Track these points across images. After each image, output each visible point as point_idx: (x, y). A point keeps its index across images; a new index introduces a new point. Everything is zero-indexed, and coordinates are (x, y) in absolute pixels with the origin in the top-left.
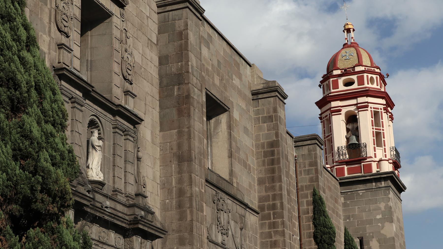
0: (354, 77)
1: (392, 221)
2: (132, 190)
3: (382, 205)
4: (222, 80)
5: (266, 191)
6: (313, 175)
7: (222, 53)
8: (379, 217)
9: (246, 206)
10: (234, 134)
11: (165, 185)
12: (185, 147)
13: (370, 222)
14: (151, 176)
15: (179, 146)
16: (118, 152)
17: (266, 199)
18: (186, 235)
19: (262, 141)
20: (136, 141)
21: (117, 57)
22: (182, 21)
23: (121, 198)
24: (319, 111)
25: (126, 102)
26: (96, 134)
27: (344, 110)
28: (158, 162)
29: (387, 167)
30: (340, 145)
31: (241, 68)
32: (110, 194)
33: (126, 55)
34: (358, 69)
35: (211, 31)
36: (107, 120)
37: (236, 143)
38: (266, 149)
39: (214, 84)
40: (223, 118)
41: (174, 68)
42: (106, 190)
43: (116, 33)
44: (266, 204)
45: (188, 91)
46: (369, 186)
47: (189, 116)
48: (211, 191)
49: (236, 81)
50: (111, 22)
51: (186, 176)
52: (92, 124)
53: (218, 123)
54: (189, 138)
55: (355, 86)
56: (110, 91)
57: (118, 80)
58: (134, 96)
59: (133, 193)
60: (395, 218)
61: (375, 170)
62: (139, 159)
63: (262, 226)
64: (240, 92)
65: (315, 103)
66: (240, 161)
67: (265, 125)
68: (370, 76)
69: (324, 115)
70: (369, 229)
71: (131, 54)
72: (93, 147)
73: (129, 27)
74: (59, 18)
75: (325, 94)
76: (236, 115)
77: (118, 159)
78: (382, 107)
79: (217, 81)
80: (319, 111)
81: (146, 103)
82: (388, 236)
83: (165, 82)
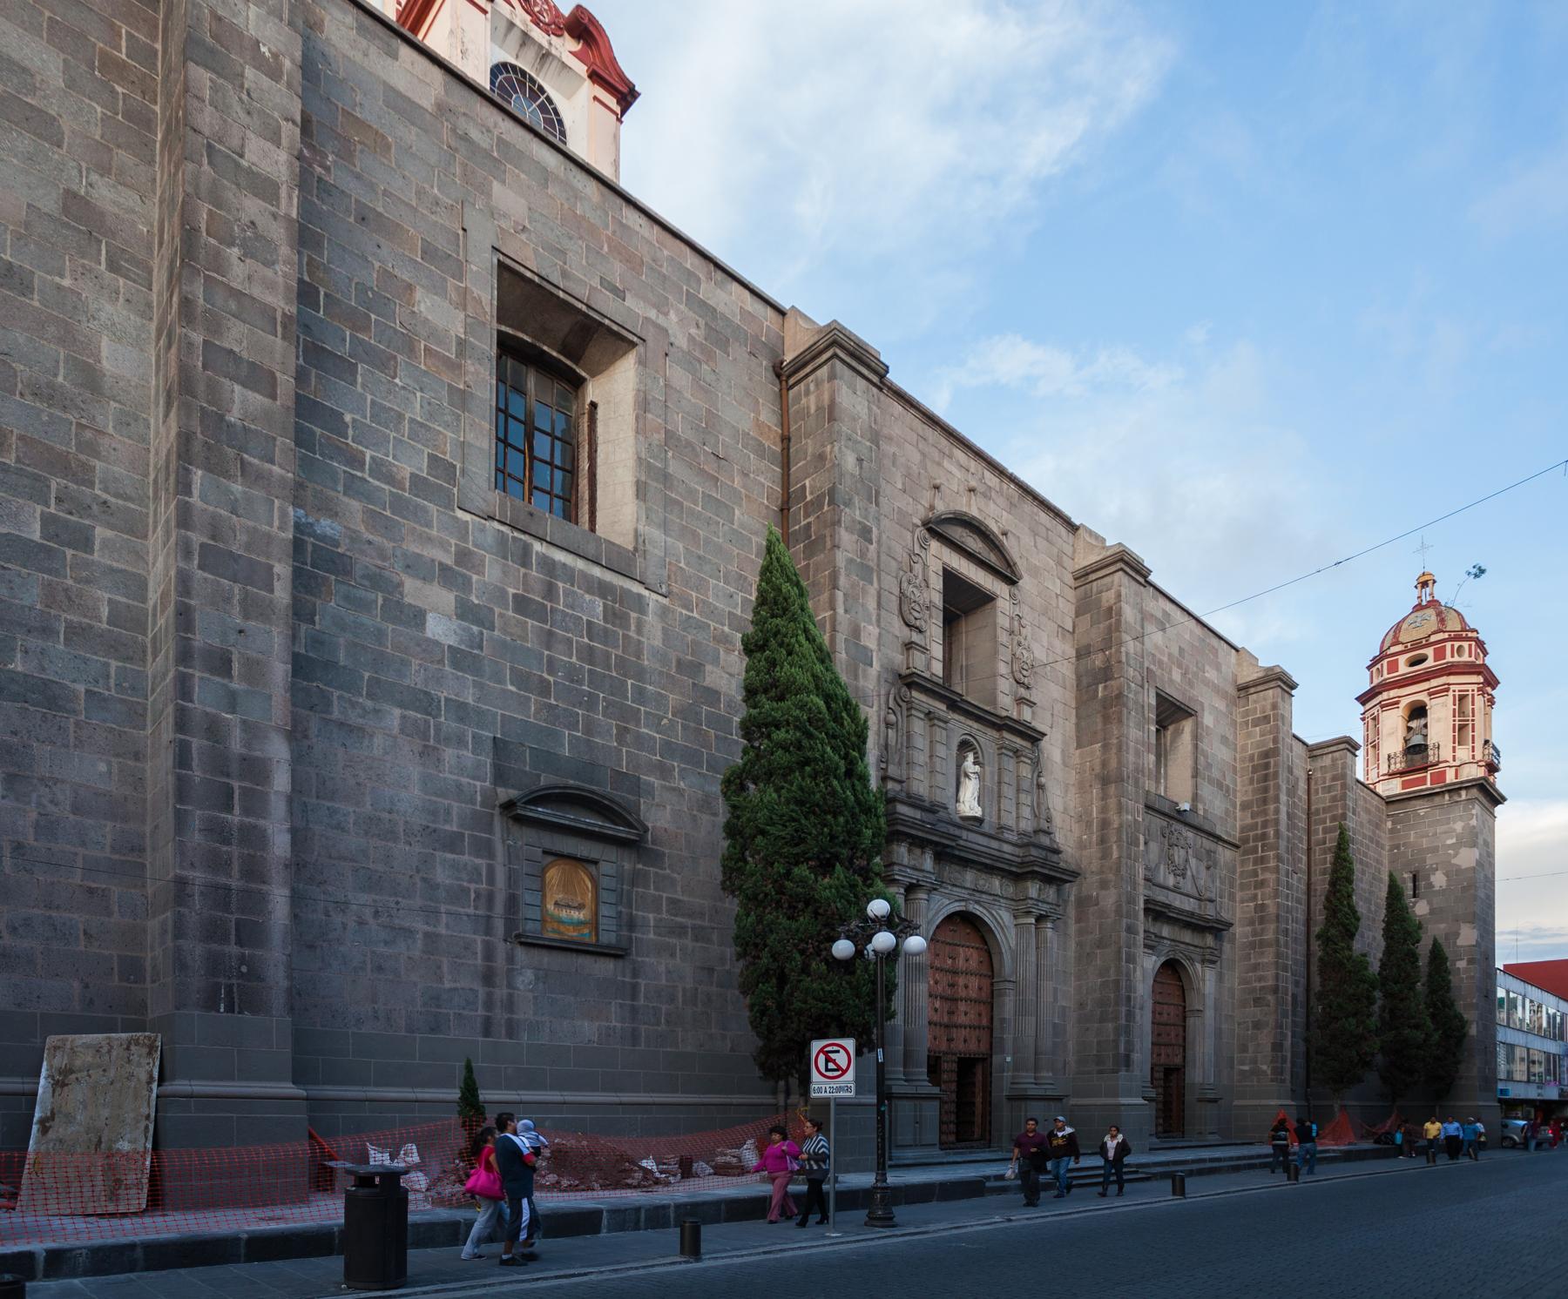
2: (1027, 825)
4: (1184, 675)
6: (1337, 792)
7: (1187, 637)
9: (1219, 838)
10: (1203, 746)
11: (1083, 819)
12: (1113, 764)
13: (1435, 850)
14: (1060, 807)
15: (1104, 764)
16: (1006, 779)
17: (1254, 827)
18: (1111, 876)
20: (1036, 764)
21: (1004, 654)
23: (1007, 835)
24: (1362, 709)
25: (1019, 713)
26: (971, 757)
28: (1073, 790)
30: (1392, 752)
31: (1221, 653)
32: (992, 832)
33: (1019, 651)
35: (1169, 607)
36: (986, 738)
37: (1206, 757)
39: (1171, 680)
40: (1187, 726)
41: (1098, 660)
42: (986, 828)
43: (1003, 621)
45: (1120, 689)
46: (1437, 800)
47: (1120, 721)
48: (1158, 822)
49: (1211, 674)
50: (994, 608)
51: (1112, 802)
52: (965, 746)
53: (1178, 733)
54: (1120, 749)
56: (994, 702)
57: (1005, 685)
58: (1031, 704)
59: (1030, 829)
60: (1480, 841)
61: (1450, 777)
62: (1040, 787)
63: (1243, 863)
64: (1217, 690)
65: (579, 7)
66: (1211, 781)
68: (1457, 644)
70: (1430, 860)
71: (1028, 649)
72: (967, 776)
73: (1025, 611)
74: (905, 608)
76: (1208, 719)
77: (1005, 788)
79: (1176, 675)
81: (1053, 710)
83: (1085, 681)
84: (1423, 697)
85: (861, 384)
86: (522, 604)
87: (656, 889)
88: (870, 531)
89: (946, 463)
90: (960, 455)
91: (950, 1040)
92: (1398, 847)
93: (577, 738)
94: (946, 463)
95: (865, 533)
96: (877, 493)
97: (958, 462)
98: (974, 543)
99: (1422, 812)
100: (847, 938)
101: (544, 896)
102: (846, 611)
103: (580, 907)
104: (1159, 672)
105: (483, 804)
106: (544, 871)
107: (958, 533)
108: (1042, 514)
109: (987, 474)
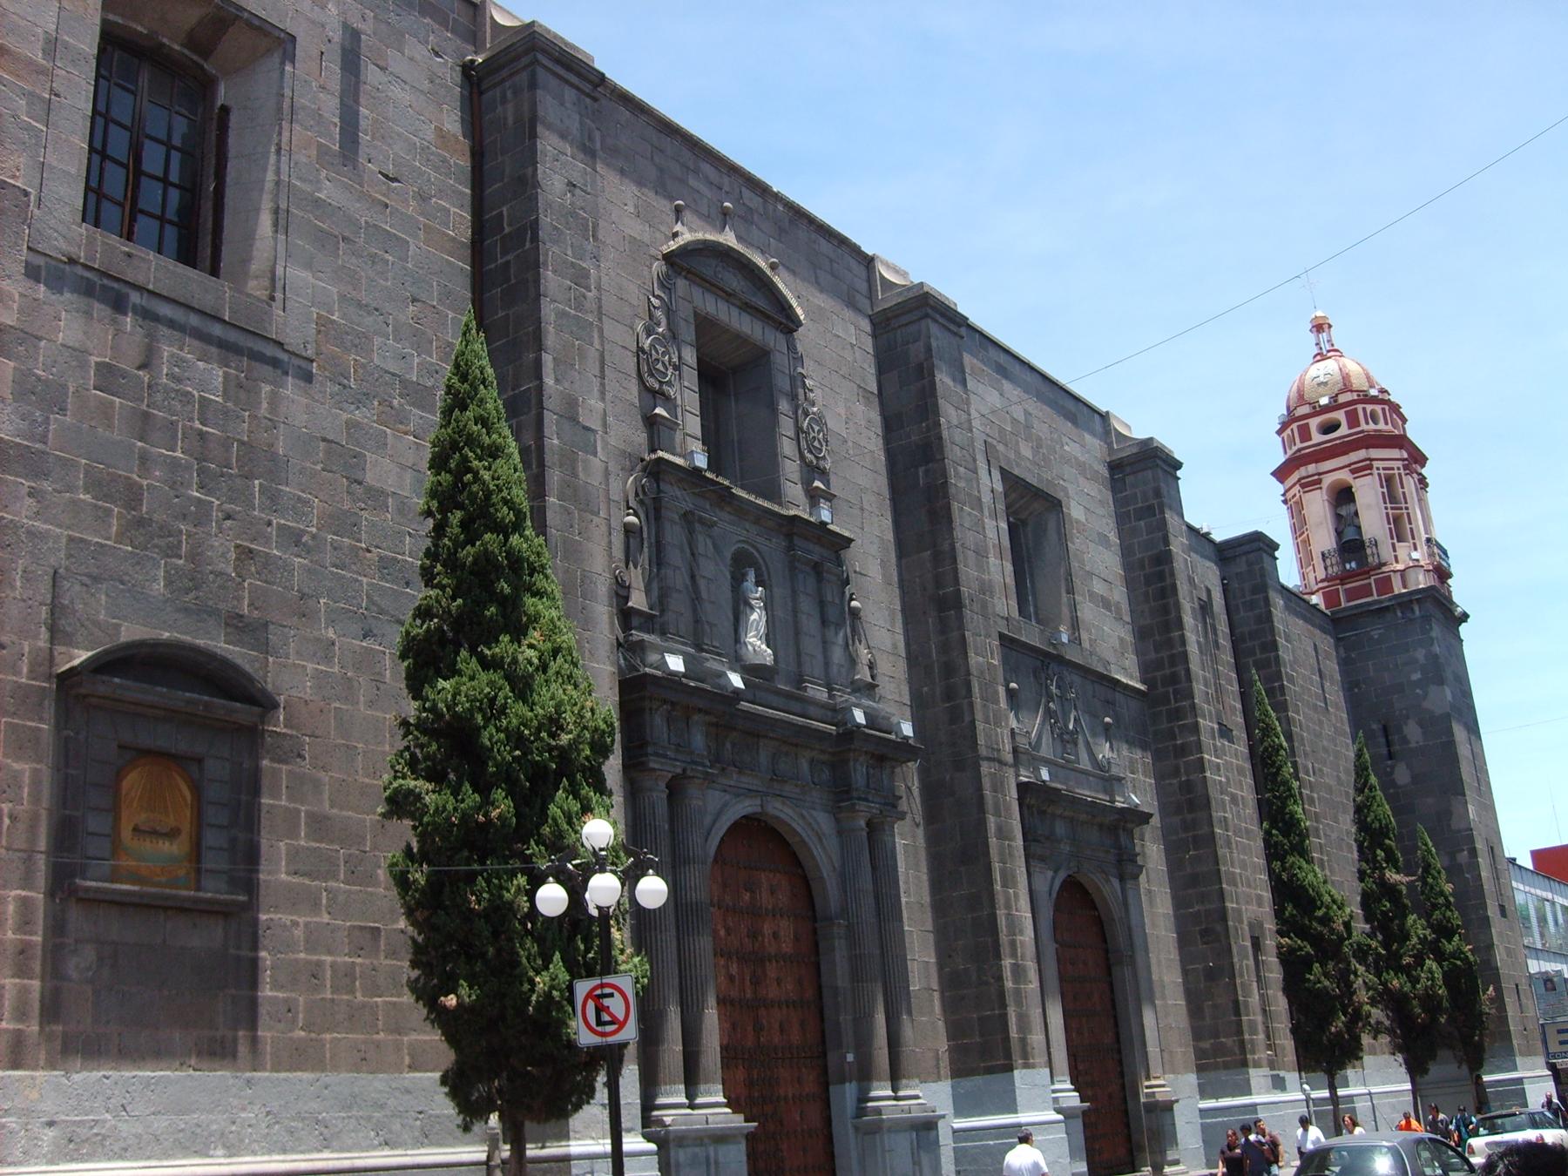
0: (1340, 415)
1: (1441, 681)
3: (1420, 654)
5: (1157, 651)
8: (1416, 676)
17: (1159, 665)
19: (1138, 556)
22: (921, 343)
24: (1280, 488)
27: (1328, 480)
29: (1422, 581)
34: (1342, 399)
38: (1148, 570)
44: (1158, 674)
52: (741, 562)
55: (1343, 430)
58: (830, 497)
67: (1142, 523)
68: (1369, 408)
69: (1289, 495)
75: (1290, 453)
78: (1400, 464)
79: (1026, 451)
80: (1280, 488)
82: (1438, 712)
84: (1344, 475)
85: (570, 94)
86: (108, 376)
87: (290, 798)
88: (587, 275)
89: (692, 182)
90: (706, 168)
91: (758, 1029)
92: (1357, 685)
93: (176, 568)
94: (692, 182)
95: (581, 278)
96: (595, 226)
97: (707, 178)
98: (734, 282)
99: (1375, 634)
100: (558, 881)
101: (117, 820)
102: (557, 381)
103: (172, 834)
104: (1001, 447)
105: (32, 674)
106: (119, 776)
107: (709, 268)
108: (823, 241)
109: (747, 193)
